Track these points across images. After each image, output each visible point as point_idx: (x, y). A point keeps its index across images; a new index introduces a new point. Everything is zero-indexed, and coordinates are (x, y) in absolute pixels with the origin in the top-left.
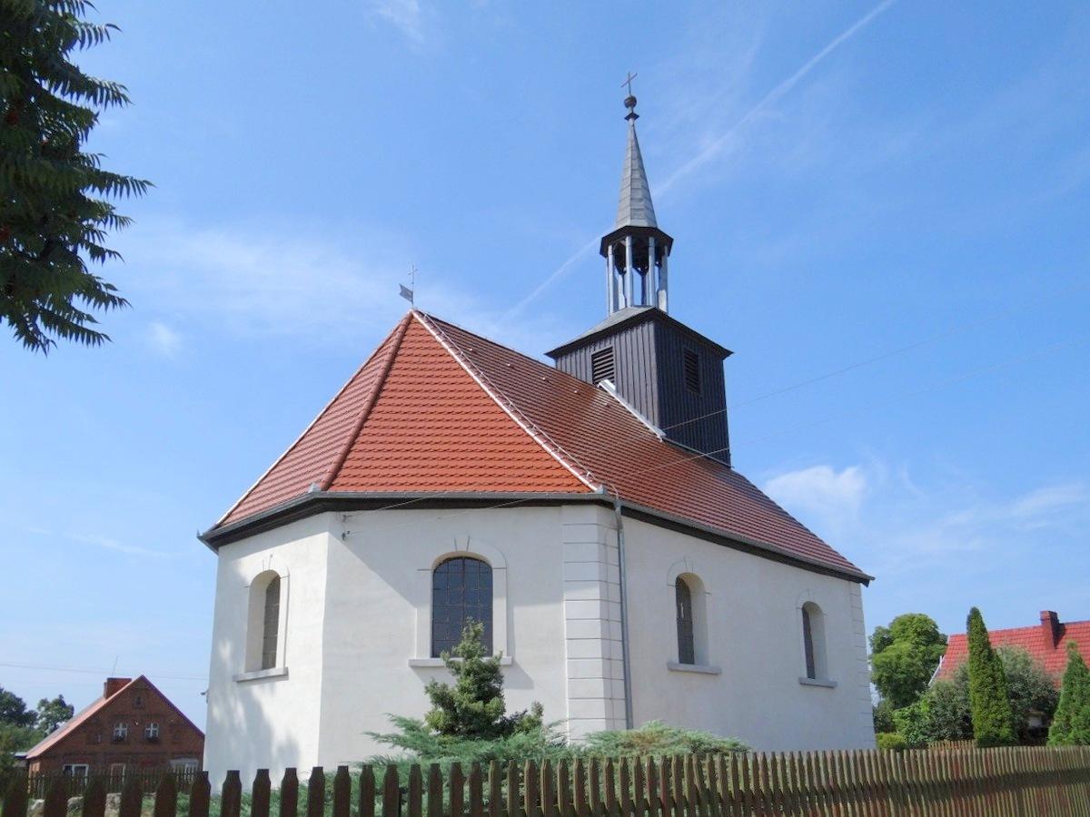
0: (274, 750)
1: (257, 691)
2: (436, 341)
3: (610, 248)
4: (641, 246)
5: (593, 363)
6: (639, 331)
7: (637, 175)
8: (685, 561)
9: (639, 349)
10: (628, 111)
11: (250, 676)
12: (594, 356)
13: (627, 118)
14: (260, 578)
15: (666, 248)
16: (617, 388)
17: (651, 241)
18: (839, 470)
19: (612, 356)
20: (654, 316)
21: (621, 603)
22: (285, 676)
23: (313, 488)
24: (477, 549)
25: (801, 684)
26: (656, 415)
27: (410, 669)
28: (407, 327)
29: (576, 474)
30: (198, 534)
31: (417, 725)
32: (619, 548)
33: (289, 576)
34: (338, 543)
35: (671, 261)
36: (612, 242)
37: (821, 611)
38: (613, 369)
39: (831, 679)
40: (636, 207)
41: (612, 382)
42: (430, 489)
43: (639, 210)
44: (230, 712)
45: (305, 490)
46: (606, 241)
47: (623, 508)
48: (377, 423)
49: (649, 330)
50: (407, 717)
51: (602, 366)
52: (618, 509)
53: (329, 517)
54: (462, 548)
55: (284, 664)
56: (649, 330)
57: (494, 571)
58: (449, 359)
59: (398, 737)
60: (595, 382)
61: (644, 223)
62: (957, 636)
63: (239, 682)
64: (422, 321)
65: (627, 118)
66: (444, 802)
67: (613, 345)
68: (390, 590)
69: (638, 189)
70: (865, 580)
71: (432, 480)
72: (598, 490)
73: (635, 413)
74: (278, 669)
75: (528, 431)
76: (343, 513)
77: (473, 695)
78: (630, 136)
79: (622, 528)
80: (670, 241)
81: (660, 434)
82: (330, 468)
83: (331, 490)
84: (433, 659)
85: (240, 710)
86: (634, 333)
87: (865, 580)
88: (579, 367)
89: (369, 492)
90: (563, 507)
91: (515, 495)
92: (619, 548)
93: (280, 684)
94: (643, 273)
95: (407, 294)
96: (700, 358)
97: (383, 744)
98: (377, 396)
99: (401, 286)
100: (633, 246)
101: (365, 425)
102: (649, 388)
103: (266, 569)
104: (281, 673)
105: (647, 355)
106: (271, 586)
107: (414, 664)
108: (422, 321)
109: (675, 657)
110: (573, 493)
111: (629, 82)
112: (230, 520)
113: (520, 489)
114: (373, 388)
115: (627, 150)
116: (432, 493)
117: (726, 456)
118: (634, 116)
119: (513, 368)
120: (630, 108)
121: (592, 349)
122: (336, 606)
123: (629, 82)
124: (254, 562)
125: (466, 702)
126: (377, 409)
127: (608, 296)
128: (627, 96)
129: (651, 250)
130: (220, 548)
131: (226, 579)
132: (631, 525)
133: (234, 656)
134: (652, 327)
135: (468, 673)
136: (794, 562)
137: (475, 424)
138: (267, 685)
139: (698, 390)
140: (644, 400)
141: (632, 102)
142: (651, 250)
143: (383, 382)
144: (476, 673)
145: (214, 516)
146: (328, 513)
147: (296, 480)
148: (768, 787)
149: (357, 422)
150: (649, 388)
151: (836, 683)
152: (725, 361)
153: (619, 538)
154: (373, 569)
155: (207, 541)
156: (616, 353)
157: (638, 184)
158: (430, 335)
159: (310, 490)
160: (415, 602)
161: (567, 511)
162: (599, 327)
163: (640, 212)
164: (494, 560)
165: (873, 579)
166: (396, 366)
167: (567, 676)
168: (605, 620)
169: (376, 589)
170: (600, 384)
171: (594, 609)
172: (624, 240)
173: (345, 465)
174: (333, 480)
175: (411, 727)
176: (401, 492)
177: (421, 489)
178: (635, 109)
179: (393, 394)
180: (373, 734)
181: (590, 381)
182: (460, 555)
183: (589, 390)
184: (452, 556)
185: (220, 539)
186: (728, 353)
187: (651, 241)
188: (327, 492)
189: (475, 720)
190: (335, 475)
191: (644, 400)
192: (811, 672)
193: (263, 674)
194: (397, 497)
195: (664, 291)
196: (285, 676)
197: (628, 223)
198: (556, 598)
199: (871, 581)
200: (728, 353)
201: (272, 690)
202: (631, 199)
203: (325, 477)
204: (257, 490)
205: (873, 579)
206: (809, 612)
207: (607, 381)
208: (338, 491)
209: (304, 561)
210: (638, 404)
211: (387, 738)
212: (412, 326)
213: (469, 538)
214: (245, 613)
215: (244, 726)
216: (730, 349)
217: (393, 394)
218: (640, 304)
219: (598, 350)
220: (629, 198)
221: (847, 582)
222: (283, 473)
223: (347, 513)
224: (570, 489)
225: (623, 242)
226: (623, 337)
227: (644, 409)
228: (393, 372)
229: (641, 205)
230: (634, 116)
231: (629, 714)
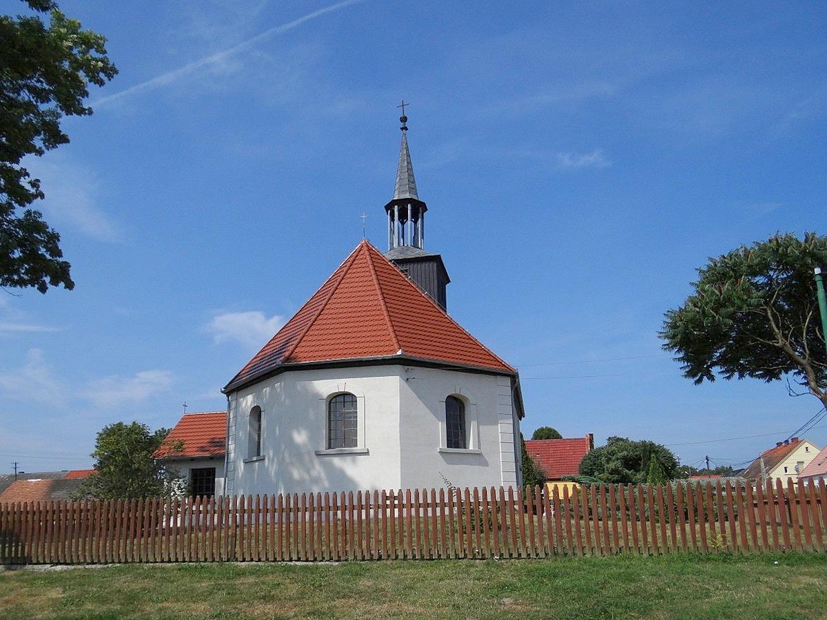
4: (409, 209)
10: (401, 125)
18: (268, 316)
25: (317, 455)
42: (431, 357)
56: (433, 266)
62: (618, 440)
65: (402, 129)
66: (446, 514)
94: (403, 223)
116: (448, 362)
128: (402, 116)
138: (349, 458)
141: (404, 119)
146: (398, 366)
148: (184, 525)
167: (501, 451)
201: (354, 461)
230: (406, 129)
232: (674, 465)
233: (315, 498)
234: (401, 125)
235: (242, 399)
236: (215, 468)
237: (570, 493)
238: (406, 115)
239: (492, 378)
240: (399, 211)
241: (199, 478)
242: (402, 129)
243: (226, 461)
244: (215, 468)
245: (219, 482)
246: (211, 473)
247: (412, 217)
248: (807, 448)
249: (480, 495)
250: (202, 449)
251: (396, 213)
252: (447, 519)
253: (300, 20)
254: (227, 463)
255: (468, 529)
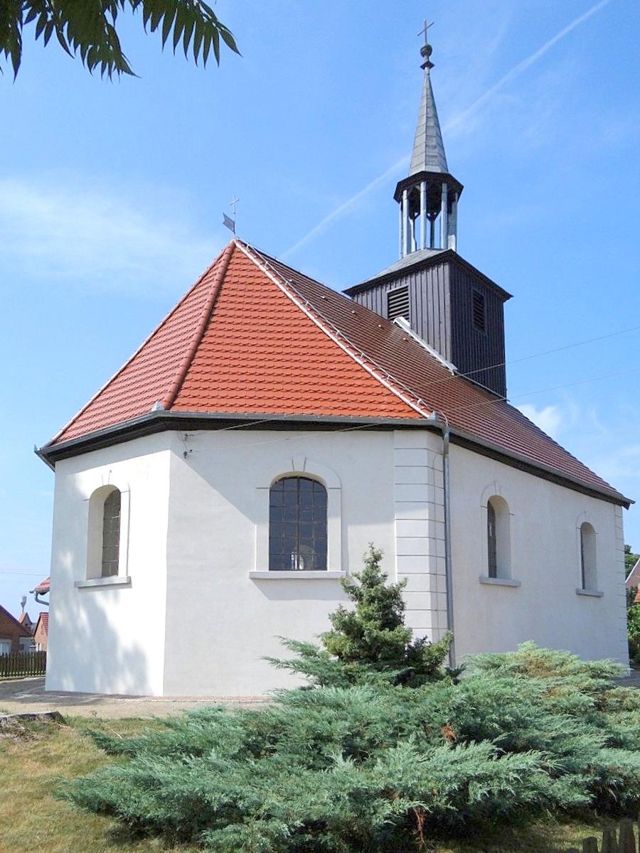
0: (120, 655)
1: (99, 596)
2: (260, 271)
3: (405, 192)
4: (433, 192)
5: (389, 301)
6: (435, 272)
7: (432, 124)
8: (495, 485)
9: (433, 291)
10: (423, 60)
11: (92, 583)
12: (389, 295)
13: (423, 67)
14: (98, 492)
15: (456, 194)
16: (411, 325)
17: (444, 187)
19: (407, 295)
20: (449, 258)
21: (445, 523)
22: (128, 584)
23: (156, 407)
24: (313, 469)
26: (449, 350)
27: (251, 581)
28: (232, 252)
29: (408, 401)
30: (36, 448)
31: (315, 650)
32: (444, 472)
33: (129, 491)
34: (181, 461)
35: (462, 204)
36: (407, 186)
37: (594, 531)
38: (408, 302)
39: (599, 590)
40: (431, 154)
41: (407, 319)
43: (433, 156)
44: (73, 618)
45: (147, 408)
46: (401, 186)
47: (451, 434)
48: (210, 347)
49: (444, 271)
50: (301, 640)
51: (398, 304)
52: (447, 435)
53: (170, 436)
54: (299, 469)
55: (127, 575)
56: (444, 271)
57: (329, 492)
58: (274, 288)
59: (298, 662)
60: (391, 318)
61: (437, 170)
63: (80, 588)
64: (245, 251)
65: (423, 67)
67: (408, 284)
68: (231, 507)
69: (432, 136)
70: (626, 504)
71: (251, 402)
72: (431, 417)
73: (428, 348)
74: (121, 577)
75: (357, 359)
76: (184, 433)
77: (378, 623)
78: (426, 84)
79: (447, 453)
80: (460, 188)
81: (452, 368)
82: (171, 388)
83: (173, 409)
84: (271, 572)
85: (83, 616)
86: (429, 274)
87: (626, 504)
88: (376, 302)
89: (211, 413)
90: (396, 431)
91: (352, 420)
92: (444, 472)
93: (123, 592)
94: (432, 219)
95: (229, 224)
96: (485, 298)
97: (282, 669)
98: (208, 321)
99: (225, 216)
100: (427, 191)
101: (199, 348)
102: (442, 326)
103: (106, 484)
104: (125, 581)
105: (441, 292)
106: (111, 501)
107: (254, 576)
108: (245, 251)
109: (487, 574)
110: (405, 418)
111: (425, 30)
112: (65, 436)
113: (355, 413)
114: (204, 313)
115: (423, 97)
117: (503, 391)
118: (429, 65)
119: (327, 300)
120: (425, 57)
121: (388, 288)
122: (180, 521)
123: (425, 30)
124: (91, 477)
125: (372, 628)
126: (209, 333)
127: (396, 240)
128: (424, 45)
129: (444, 196)
130: (57, 463)
131: (63, 492)
132: (455, 450)
133: (76, 564)
134: (447, 267)
135: (372, 600)
136: (582, 490)
137: (227, 362)
138: (111, 592)
139: (483, 328)
140: (437, 336)
141: (427, 51)
142: (444, 196)
143: (213, 308)
144: (380, 600)
145: (47, 435)
147: (134, 399)
149: (192, 345)
150: (442, 326)
151: (520, 582)
152: (504, 304)
153: (444, 462)
154: (214, 485)
155: (44, 455)
156: (412, 292)
157: (433, 132)
158: (254, 264)
159: (154, 409)
160: (254, 519)
161: (398, 434)
162: (395, 268)
163: (434, 159)
164: (329, 482)
165: (634, 502)
166: (223, 292)
168: (433, 538)
169: (217, 505)
170: (395, 320)
171: (423, 528)
172: (420, 186)
173: (185, 385)
174: (174, 400)
175: (308, 652)
176: (242, 413)
177: (260, 411)
178: (430, 58)
179: (222, 319)
180: (272, 660)
181: (385, 316)
182: (295, 475)
183: (387, 323)
184: (288, 476)
185: (55, 454)
186: (508, 296)
187: (444, 187)
188: (171, 410)
189: (385, 648)
190: (175, 396)
191: (437, 336)
192: (493, 571)
193: (107, 581)
194: (239, 418)
195: (453, 236)
196: (128, 584)
197: (423, 168)
198: (388, 519)
199: (631, 505)
200: (508, 296)
201: (116, 597)
202: (426, 146)
203: (167, 396)
204: (91, 408)
205: (634, 502)
206: (586, 529)
207: (402, 319)
208: (178, 411)
209: (147, 478)
210: (431, 341)
211: (287, 664)
212: (235, 255)
213: (306, 459)
214: (85, 529)
215: (88, 630)
216: (510, 293)
217: (222, 319)
218: (429, 247)
219: (393, 289)
220: (424, 144)
221: (612, 505)
222: (117, 393)
223: (188, 432)
224: (403, 415)
225: (417, 187)
226: (418, 277)
227: (437, 345)
228: (221, 299)
229: (435, 152)
230: (429, 65)
231: (451, 624)
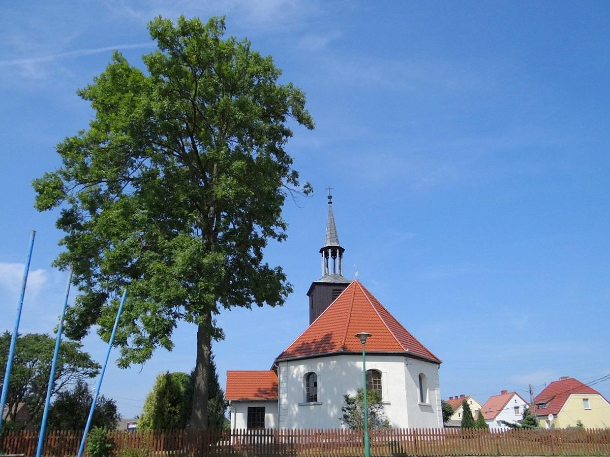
4: (335, 252)
65: (329, 203)
94: (334, 259)
141: (330, 197)
232: (381, 399)
233: (341, 431)
234: (328, 200)
235: (293, 367)
236: (264, 407)
237: (506, 430)
238: (331, 195)
239: (431, 364)
240: (332, 253)
241: (252, 413)
242: (329, 203)
243: (278, 403)
244: (264, 407)
245: (268, 418)
246: (262, 411)
247: (332, 255)
248: (515, 400)
249: (500, 430)
250: (256, 395)
251: (330, 254)
252: (429, 442)
253: (104, 49)
254: (280, 404)
255: (346, 445)
